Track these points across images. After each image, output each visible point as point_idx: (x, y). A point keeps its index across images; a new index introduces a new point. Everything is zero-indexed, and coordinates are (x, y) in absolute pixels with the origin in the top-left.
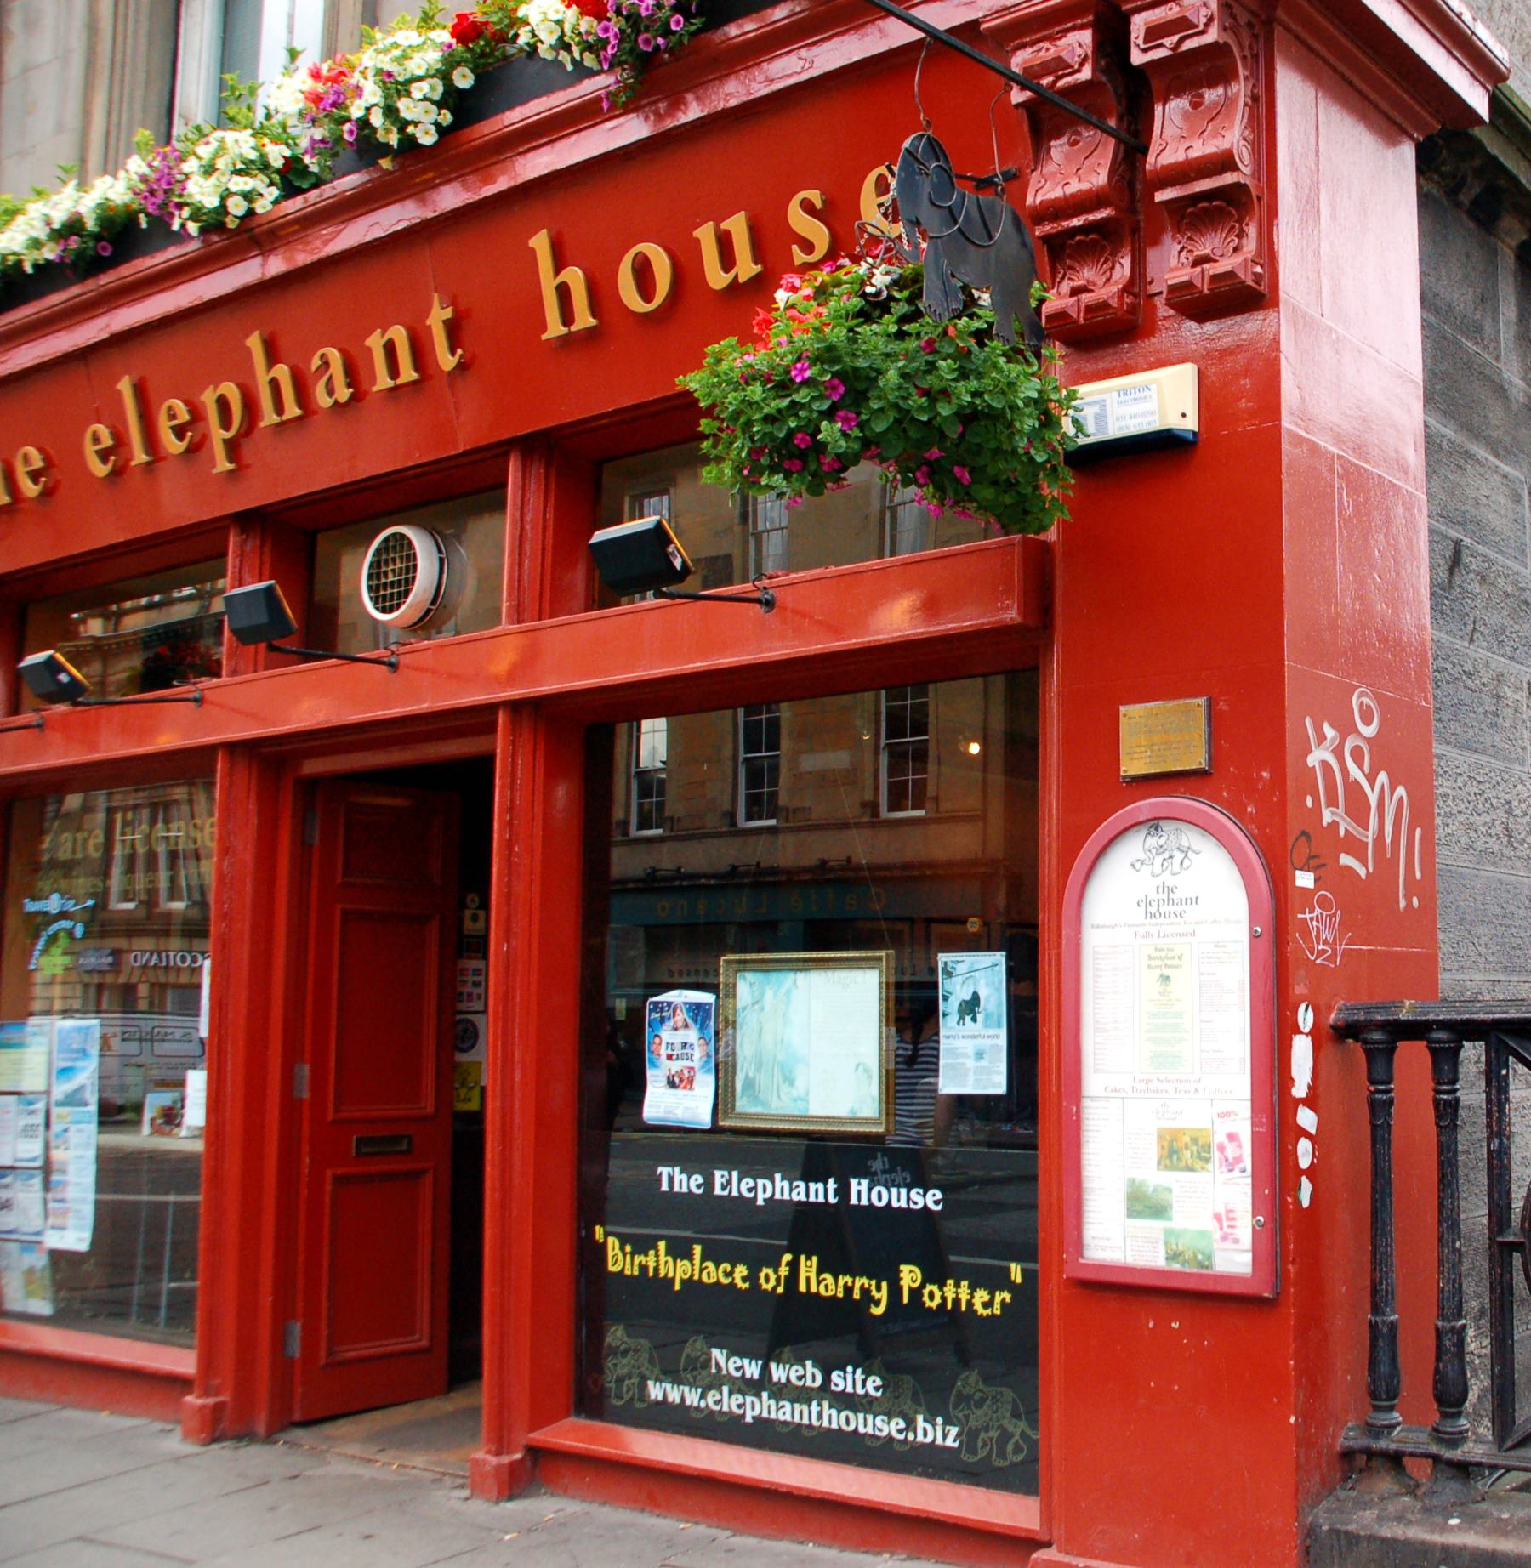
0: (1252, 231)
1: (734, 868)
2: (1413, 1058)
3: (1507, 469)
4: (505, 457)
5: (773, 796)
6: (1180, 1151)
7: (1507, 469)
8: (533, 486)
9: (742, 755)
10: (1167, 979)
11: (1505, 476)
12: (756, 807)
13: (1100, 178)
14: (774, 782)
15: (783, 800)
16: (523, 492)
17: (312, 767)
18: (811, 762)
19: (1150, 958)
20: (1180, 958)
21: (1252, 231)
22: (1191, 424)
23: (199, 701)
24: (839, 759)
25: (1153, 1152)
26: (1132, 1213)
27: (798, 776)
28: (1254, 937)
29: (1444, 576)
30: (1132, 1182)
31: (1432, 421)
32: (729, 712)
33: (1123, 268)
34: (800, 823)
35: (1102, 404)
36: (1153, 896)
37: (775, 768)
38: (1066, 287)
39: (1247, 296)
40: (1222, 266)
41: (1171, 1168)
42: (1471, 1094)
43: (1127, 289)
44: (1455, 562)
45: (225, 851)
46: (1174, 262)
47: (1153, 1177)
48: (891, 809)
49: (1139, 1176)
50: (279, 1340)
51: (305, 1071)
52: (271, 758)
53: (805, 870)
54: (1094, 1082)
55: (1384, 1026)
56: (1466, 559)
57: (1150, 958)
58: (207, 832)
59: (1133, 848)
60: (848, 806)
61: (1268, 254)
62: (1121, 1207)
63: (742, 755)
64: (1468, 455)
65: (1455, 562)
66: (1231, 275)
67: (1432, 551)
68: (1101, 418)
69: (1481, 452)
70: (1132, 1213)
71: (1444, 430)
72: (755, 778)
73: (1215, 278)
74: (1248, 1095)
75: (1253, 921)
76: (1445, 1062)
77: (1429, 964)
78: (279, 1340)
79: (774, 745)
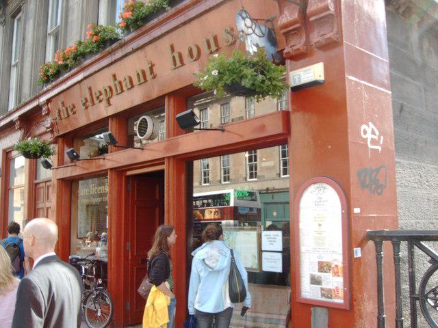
0: (335, 26)
1: (268, 189)
2: (387, 246)
3: (416, 83)
4: (164, 98)
5: (256, 173)
6: (323, 267)
7: (416, 83)
8: (171, 103)
9: (247, 163)
10: (320, 225)
11: (416, 85)
12: (251, 176)
13: (296, 15)
14: (256, 169)
15: (258, 174)
16: (169, 105)
17: (129, 173)
18: (264, 164)
19: (315, 218)
20: (325, 218)
21: (335, 26)
22: (322, 78)
23: (104, 159)
24: (271, 164)
25: (317, 267)
26: (312, 283)
27: (261, 168)
28: (343, 214)
29: (398, 113)
30: (312, 275)
31: (393, 72)
32: (278, 147)
33: (304, 39)
34: (262, 178)
35: (299, 75)
36: (317, 200)
37: (256, 167)
38: (289, 46)
39: (332, 45)
40: (328, 36)
41: (322, 272)
42: (404, 253)
43: (305, 44)
44: (401, 109)
45: (111, 193)
46: (316, 36)
47: (317, 273)
48: (284, 174)
49: (313, 273)
50: (125, 305)
51: (129, 244)
52: (120, 171)
53: (264, 190)
54: (303, 249)
55: (380, 236)
56: (405, 108)
57: (315, 218)
58: (107, 189)
59: (312, 188)
60: (274, 174)
61: (340, 31)
62: (309, 282)
63: (247, 163)
64: (403, 80)
65: (401, 109)
66: (330, 38)
67: (393, 108)
68: (299, 78)
69: (408, 79)
70: (312, 283)
71: (397, 74)
72: (251, 169)
73: (326, 39)
74: (341, 252)
75: (342, 209)
76: (396, 247)
77: (395, 220)
78: (125, 305)
79: (255, 160)
